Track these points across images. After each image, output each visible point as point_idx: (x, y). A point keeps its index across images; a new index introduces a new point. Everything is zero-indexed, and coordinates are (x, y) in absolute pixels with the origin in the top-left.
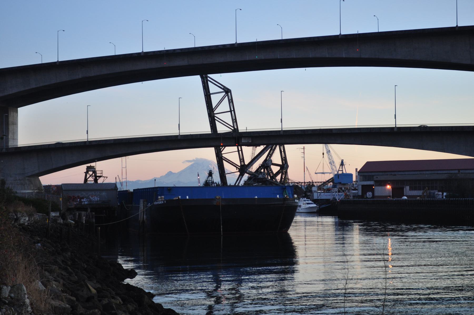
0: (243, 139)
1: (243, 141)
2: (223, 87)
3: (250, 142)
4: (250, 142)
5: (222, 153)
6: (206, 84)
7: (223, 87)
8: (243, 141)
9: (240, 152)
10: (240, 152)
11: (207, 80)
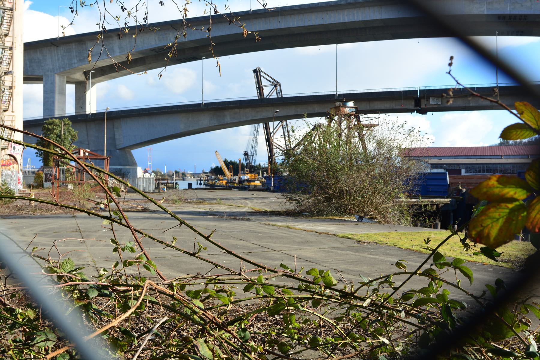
0: (431, 99)
1: (431, 103)
3: (440, 103)
7: (272, 81)
8: (431, 103)
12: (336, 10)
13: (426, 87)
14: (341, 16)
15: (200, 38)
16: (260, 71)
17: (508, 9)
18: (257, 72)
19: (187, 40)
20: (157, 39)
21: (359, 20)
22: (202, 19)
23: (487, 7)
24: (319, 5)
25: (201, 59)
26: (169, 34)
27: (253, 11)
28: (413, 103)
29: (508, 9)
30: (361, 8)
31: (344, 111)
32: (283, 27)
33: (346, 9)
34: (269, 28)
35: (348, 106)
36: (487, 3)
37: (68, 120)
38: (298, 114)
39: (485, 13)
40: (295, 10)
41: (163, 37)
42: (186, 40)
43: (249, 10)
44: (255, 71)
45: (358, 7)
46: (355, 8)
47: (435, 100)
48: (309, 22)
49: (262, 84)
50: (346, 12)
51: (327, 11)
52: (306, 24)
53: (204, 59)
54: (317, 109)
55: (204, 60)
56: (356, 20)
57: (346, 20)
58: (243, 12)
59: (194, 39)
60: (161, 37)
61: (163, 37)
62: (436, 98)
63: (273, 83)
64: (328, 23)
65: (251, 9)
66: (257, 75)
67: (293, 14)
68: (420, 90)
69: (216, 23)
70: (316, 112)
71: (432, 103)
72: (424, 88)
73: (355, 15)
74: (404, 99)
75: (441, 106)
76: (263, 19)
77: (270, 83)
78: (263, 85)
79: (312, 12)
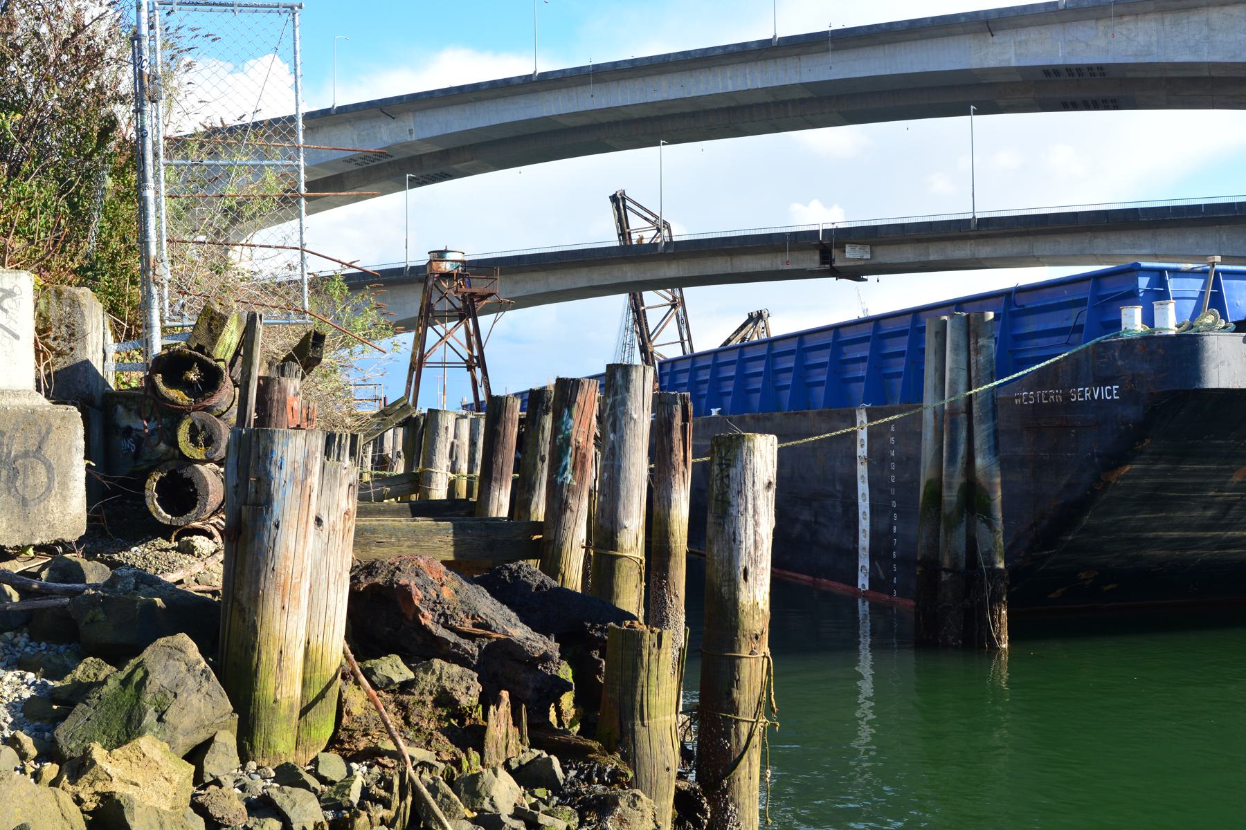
0: (848, 248)
2: (653, 219)
3: (868, 256)
4: (868, 256)
5: (654, 344)
6: (623, 211)
7: (653, 219)
8: (848, 255)
9: (687, 343)
10: (687, 343)
11: (624, 205)
12: (709, 68)
13: (833, 224)
14: (719, 79)
15: (440, 134)
16: (624, 199)
17: (1060, 55)
18: (618, 200)
19: (414, 138)
20: (355, 137)
21: (755, 87)
22: (441, 95)
23: (1015, 50)
24: (671, 59)
25: (658, 144)
26: (380, 127)
27: (541, 74)
28: (817, 257)
29: (1060, 55)
30: (759, 63)
31: (439, 267)
32: (604, 106)
33: (728, 65)
34: (576, 110)
35: (448, 259)
36: (1015, 43)
37: (871, 708)
38: (595, 284)
39: (1014, 63)
40: (624, 70)
41: (368, 134)
42: (414, 139)
43: (532, 72)
44: (614, 198)
45: (752, 60)
46: (747, 62)
47: (857, 249)
48: (655, 95)
49: (628, 227)
50: (729, 71)
51: (691, 70)
52: (650, 100)
53: (664, 144)
54: (629, 274)
55: (663, 147)
56: (749, 87)
57: (730, 89)
58: (520, 77)
59: (429, 136)
60: (363, 133)
61: (368, 134)
62: (859, 246)
63: (653, 223)
64: (693, 94)
65: (535, 72)
66: (618, 208)
67: (623, 79)
68: (823, 230)
69: (471, 102)
70: (629, 280)
71: (851, 257)
72: (830, 227)
73: (748, 76)
74: (792, 250)
75: (872, 262)
76: (564, 90)
77: (648, 224)
78: (631, 227)
79: (661, 73)
